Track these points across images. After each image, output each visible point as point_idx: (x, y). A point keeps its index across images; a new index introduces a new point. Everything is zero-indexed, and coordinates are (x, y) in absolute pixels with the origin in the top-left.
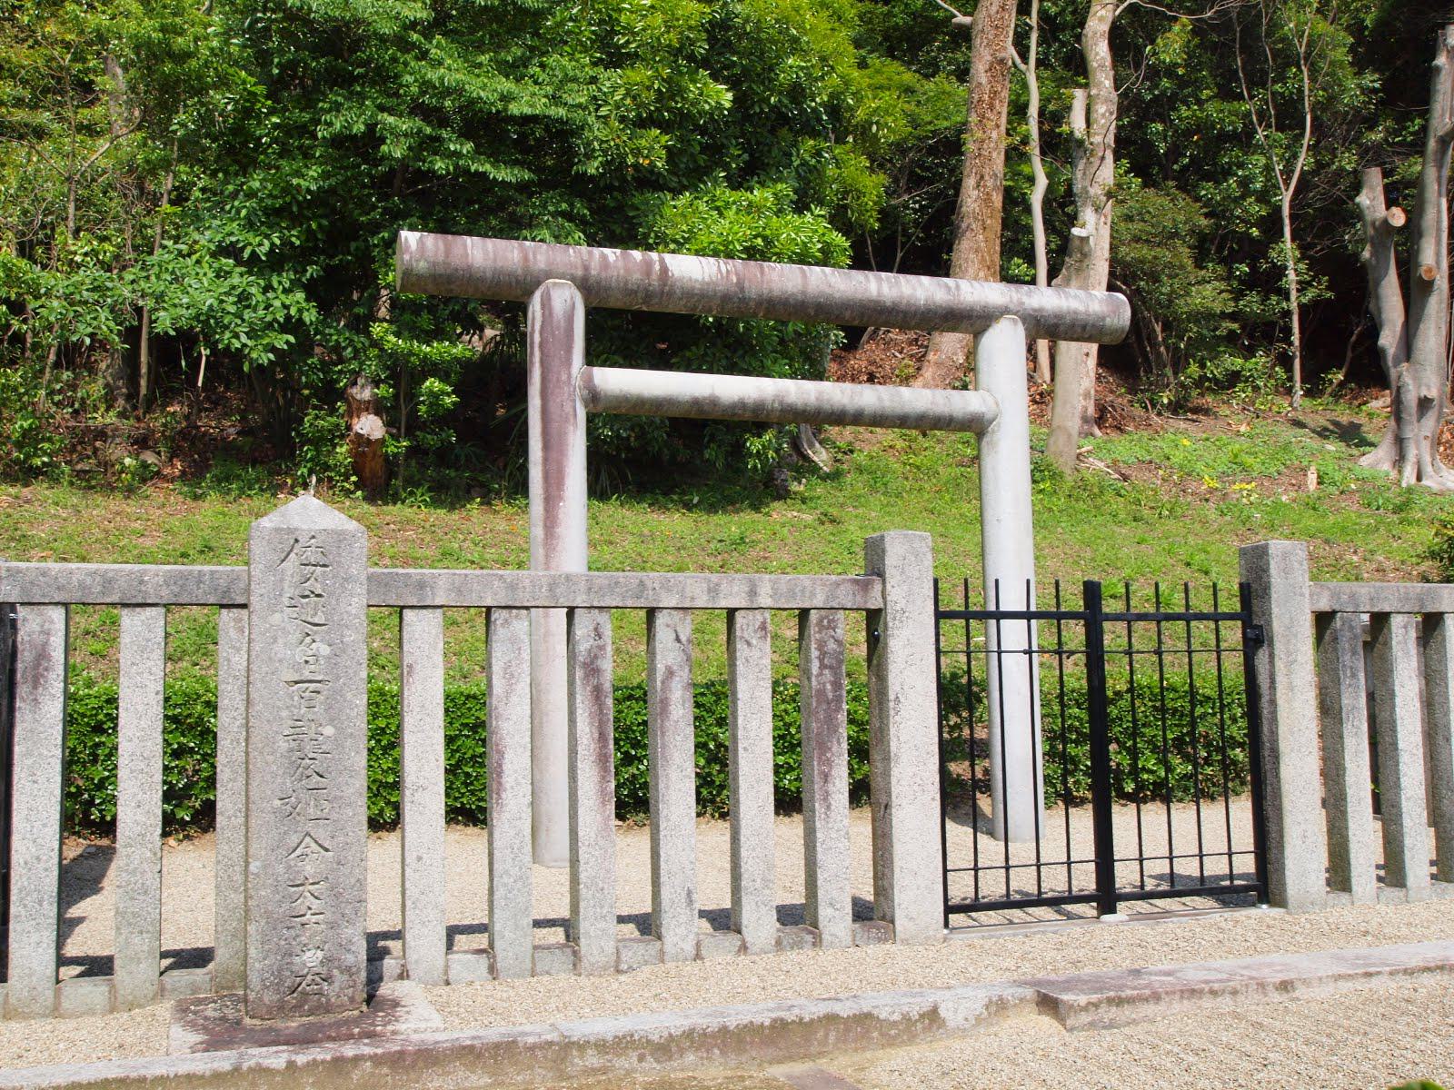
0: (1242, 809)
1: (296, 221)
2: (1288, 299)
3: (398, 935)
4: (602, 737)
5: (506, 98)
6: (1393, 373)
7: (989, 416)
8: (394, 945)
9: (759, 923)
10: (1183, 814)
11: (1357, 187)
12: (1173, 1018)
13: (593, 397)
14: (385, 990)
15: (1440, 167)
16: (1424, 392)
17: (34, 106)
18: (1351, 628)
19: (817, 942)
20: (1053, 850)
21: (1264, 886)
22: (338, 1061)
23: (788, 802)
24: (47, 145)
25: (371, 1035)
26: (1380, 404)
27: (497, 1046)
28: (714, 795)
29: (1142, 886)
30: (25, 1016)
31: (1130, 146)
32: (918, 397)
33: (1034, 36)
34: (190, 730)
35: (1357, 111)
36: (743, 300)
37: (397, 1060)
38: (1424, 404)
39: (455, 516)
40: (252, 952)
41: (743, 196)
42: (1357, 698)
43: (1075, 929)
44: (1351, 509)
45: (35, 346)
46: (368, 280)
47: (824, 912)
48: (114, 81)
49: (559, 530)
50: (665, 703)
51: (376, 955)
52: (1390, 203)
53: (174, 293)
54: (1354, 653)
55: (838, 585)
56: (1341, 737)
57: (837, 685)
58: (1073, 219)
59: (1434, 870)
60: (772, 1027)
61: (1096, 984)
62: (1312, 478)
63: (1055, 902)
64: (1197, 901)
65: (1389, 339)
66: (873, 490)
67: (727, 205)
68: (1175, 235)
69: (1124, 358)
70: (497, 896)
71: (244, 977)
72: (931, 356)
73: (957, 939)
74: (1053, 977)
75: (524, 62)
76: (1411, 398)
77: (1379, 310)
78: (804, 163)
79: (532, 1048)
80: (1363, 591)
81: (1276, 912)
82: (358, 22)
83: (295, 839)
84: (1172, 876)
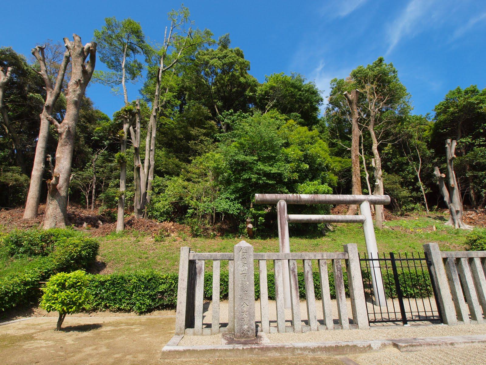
0: (433, 300)
1: (238, 192)
2: (422, 193)
3: (260, 322)
4: (296, 284)
5: (271, 170)
6: (449, 206)
7: (364, 220)
8: (259, 324)
9: (330, 323)
10: (419, 301)
11: (433, 170)
12: (425, 350)
13: (289, 220)
14: (258, 334)
15: (451, 165)
16: (457, 209)
17: (199, 178)
18: (452, 261)
19: (342, 328)
20: (391, 310)
21: (441, 319)
22: (251, 348)
23: (333, 297)
24: (200, 184)
25: (257, 343)
26: (447, 212)
27: (281, 347)
28: (319, 296)
29: (412, 318)
30: (197, 335)
31: (384, 167)
32: (349, 217)
33: (363, 150)
34: (224, 282)
35: (430, 157)
36: (315, 201)
37: (262, 349)
38: (457, 212)
39: (265, 241)
40: (235, 325)
41: (312, 183)
42: (456, 276)
43: (399, 328)
44: (444, 234)
45: (198, 215)
46: (249, 201)
47: (343, 322)
48: (210, 174)
49: (284, 244)
50: (307, 277)
51: (257, 326)
52: (441, 173)
53: (220, 206)
54: (454, 266)
55: (339, 254)
56: (454, 285)
57: (341, 274)
58: (375, 181)
59: (483, 316)
60: (335, 347)
61: (406, 341)
62: (434, 228)
63: (393, 321)
64: (426, 322)
65: (446, 199)
66: (342, 234)
67: (309, 184)
68: (396, 182)
69: (389, 207)
70: (278, 315)
71: (234, 330)
72: (350, 208)
73: (372, 329)
74: (395, 339)
75: (273, 164)
76: (454, 210)
77: (443, 193)
78: (322, 176)
79: (288, 348)
80: (453, 253)
81: (445, 325)
82: (246, 161)
83: (242, 303)
84: (419, 316)
